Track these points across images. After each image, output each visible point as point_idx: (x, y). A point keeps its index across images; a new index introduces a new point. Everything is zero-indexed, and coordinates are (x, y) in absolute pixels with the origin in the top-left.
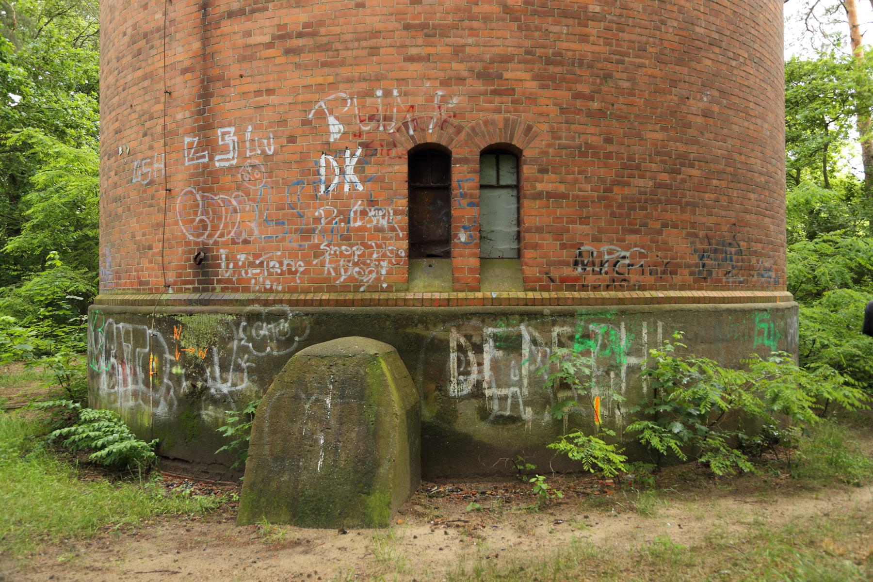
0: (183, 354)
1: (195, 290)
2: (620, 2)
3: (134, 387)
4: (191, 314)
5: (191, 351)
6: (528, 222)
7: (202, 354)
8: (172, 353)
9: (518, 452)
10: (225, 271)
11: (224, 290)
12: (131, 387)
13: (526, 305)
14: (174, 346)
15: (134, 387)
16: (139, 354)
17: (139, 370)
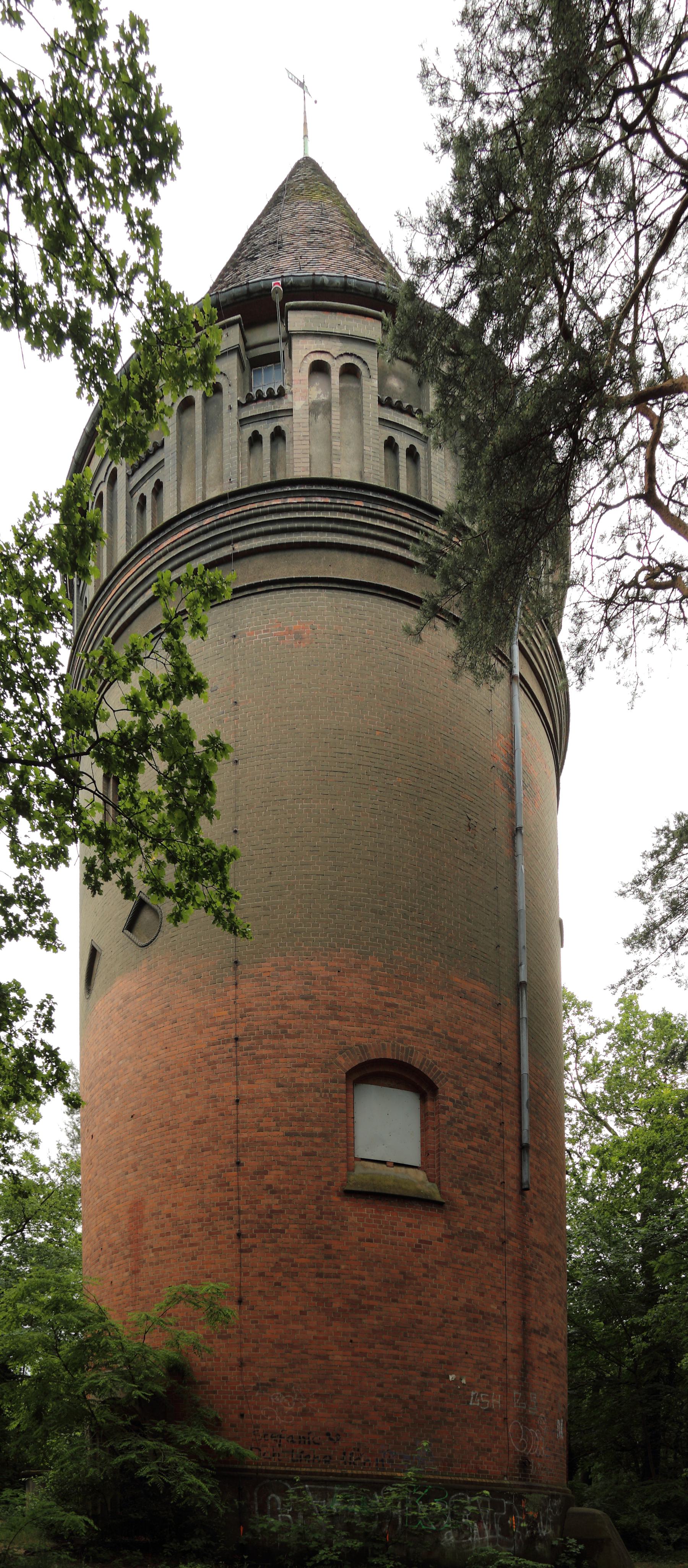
0: (527, 1516)
1: (520, 1480)
2: (686, 1166)
4: (530, 1493)
5: (531, 1514)
6: (586, 593)
7: (536, 1516)
8: (521, 1515)
10: (533, 1471)
12: (488, 1536)
13: (525, 787)
14: (522, 1511)
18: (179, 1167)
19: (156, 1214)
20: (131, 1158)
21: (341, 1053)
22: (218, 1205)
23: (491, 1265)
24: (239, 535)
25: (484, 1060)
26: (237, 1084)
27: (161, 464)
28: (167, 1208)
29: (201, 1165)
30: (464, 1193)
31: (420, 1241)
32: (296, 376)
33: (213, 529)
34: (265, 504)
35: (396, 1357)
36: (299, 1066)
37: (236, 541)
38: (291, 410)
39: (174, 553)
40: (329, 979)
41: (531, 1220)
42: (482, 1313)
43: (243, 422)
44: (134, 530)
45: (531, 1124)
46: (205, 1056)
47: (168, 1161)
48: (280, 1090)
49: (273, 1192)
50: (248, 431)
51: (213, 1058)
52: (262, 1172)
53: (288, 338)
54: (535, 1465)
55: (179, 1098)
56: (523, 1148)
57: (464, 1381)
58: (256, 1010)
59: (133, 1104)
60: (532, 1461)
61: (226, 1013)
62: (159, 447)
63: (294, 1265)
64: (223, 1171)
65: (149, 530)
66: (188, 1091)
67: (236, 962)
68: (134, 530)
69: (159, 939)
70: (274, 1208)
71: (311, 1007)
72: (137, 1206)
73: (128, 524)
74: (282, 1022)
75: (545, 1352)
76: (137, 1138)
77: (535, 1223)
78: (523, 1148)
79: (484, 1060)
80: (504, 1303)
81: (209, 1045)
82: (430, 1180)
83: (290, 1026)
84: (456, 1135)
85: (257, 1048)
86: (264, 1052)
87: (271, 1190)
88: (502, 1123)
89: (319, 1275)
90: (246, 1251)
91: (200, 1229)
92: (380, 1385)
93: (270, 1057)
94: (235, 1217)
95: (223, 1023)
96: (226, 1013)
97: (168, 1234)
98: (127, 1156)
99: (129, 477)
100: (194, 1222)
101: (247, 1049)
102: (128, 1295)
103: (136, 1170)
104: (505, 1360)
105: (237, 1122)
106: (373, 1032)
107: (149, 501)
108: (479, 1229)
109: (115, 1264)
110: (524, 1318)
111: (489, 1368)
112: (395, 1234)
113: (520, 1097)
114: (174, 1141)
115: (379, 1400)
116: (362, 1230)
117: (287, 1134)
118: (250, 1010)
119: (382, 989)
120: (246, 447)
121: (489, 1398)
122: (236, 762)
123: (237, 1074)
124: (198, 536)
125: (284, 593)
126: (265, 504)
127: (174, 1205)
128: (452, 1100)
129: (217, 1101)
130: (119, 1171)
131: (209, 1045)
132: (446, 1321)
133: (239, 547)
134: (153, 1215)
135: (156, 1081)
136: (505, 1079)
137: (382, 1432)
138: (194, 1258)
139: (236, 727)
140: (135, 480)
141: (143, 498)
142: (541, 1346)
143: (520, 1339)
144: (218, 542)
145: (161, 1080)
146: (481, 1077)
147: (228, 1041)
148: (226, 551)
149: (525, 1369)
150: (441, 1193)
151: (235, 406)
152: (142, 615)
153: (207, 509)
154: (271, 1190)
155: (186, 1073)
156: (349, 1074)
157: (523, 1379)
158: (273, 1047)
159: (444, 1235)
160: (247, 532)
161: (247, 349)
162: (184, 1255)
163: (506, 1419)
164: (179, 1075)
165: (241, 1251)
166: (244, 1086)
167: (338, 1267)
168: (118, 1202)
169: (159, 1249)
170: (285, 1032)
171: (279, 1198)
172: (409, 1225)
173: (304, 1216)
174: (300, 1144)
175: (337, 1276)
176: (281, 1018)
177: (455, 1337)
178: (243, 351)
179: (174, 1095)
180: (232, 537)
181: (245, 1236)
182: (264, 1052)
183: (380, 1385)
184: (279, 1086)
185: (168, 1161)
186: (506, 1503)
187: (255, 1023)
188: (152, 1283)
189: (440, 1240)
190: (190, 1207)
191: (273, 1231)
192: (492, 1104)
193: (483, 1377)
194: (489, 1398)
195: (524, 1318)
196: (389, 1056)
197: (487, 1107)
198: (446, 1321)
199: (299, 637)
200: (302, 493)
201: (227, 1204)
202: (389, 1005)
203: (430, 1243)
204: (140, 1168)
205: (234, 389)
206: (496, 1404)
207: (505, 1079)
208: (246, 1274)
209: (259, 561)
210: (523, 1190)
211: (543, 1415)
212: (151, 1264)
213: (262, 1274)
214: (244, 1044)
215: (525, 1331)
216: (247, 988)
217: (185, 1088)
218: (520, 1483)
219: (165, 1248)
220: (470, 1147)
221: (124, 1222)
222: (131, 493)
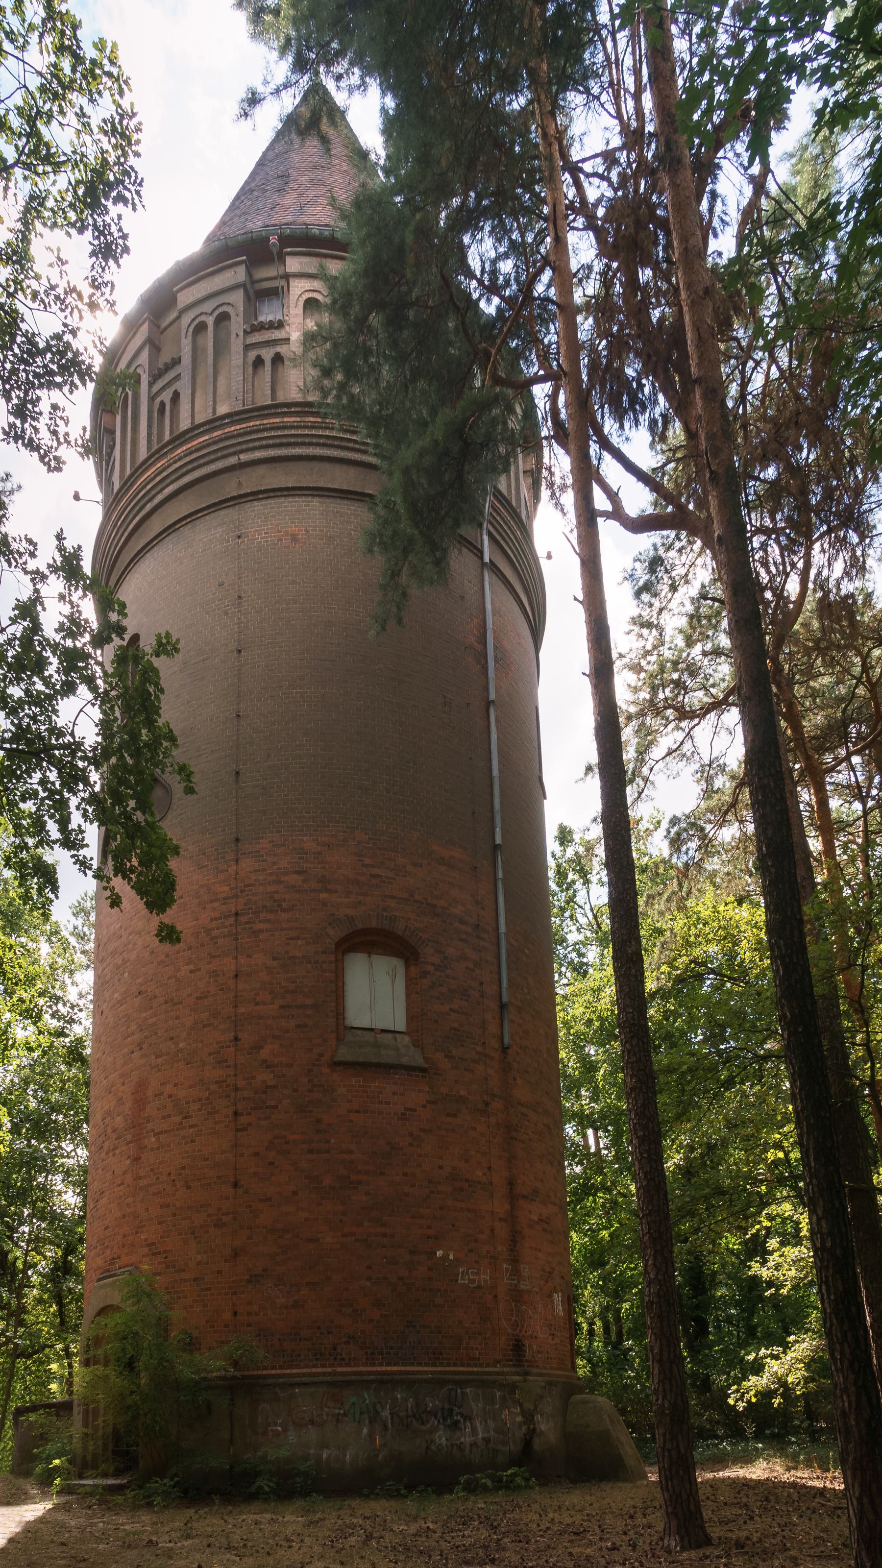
1: (514, 1366)
10: (528, 1355)
18: (181, 1045)
19: (158, 1095)
20: (137, 1037)
21: (330, 924)
22: (217, 1082)
23: (475, 1129)
24: (244, 447)
25: (462, 922)
26: (236, 958)
27: (178, 377)
28: (169, 1088)
29: (202, 1041)
30: (446, 1056)
31: (406, 1109)
32: (293, 311)
33: (221, 440)
34: (265, 422)
35: (384, 1235)
36: (292, 939)
37: (242, 452)
38: (289, 339)
39: (188, 459)
40: (319, 853)
41: (515, 1079)
42: (467, 1181)
43: (247, 348)
44: (155, 439)
45: (509, 981)
46: (208, 931)
47: (172, 1038)
48: (275, 963)
49: (268, 1067)
50: (252, 355)
51: (215, 933)
52: (257, 1047)
53: (287, 277)
54: (530, 1347)
55: (183, 973)
56: (502, 1007)
57: (451, 1257)
58: (253, 885)
59: (140, 980)
60: (527, 1343)
61: (227, 888)
62: (177, 361)
63: (287, 1143)
64: (222, 1047)
65: (167, 437)
66: (191, 967)
67: (237, 840)
68: (155, 439)
69: (169, 816)
70: (270, 1083)
71: (304, 881)
72: (141, 1086)
73: (150, 426)
74: (277, 897)
75: (535, 1218)
76: (144, 1015)
77: (519, 1081)
78: (502, 1007)
79: (462, 922)
80: (489, 1168)
81: (212, 920)
82: (414, 1046)
83: (284, 900)
84: (438, 998)
85: (254, 922)
86: (261, 926)
87: (267, 1065)
88: (481, 984)
89: (311, 1152)
90: (244, 1129)
91: (200, 1110)
92: (369, 1267)
93: (267, 931)
94: (232, 1094)
95: (225, 899)
96: (227, 888)
97: (169, 1116)
98: (133, 1034)
99: (151, 384)
100: (194, 1101)
101: (246, 923)
102: (129, 1186)
103: (141, 1049)
104: (492, 1230)
105: (236, 996)
106: (360, 902)
107: (168, 408)
108: (463, 1093)
109: (117, 1152)
110: (511, 1183)
111: (476, 1241)
112: (381, 1103)
113: (498, 956)
114: (177, 1018)
115: (368, 1284)
116: (349, 1101)
117: (281, 1007)
118: (249, 885)
119: (367, 861)
120: (250, 369)
121: (478, 1274)
122: (240, 651)
123: (237, 948)
124: (209, 445)
125: (282, 499)
126: (265, 422)
127: (176, 1085)
128: (433, 964)
129: (218, 975)
130: (126, 1050)
131: (212, 920)
132: (432, 1192)
133: (244, 457)
134: (156, 1095)
135: (163, 957)
136: (483, 939)
137: (371, 1321)
138: (193, 1141)
139: (239, 619)
140: (156, 388)
141: (162, 404)
142: (530, 1212)
143: (507, 1207)
144: (225, 452)
145: (167, 956)
146: (461, 940)
147: (229, 916)
148: (233, 460)
149: (515, 1238)
150: (425, 1058)
151: (241, 334)
152: (160, 510)
153: (217, 424)
154: (267, 1065)
155: (190, 948)
156: (338, 945)
157: (512, 1250)
158: (269, 921)
159: (428, 1102)
160: (251, 445)
161: (253, 282)
162: (184, 1138)
163: (495, 1296)
164: (184, 950)
165: (237, 1130)
166: (242, 960)
167: (328, 1142)
168: (123, 1084)
169: (160, 1133)
170: (280, 906)
171: (273, 1072)
172: (394, 1093)
173: (296, 1090)
174: (293, 1016)
175: (328, 1152)
176: (277, 892)
177: (441, 1208)
178: (248, 286)
179: (179, 970)
180: (238, 448)
181: (242, 1115)
182: (261, 926)
183: (369, 1267)
184: (274, 959)
185: (172, 1038)
186: (498, 1394)
187: (254, 898)
188: (152, 1170)
189: (424, 1106)
190: (191, 1087)
191: (267, 1107)
192: (471, 966)
193: (471, 1251)
194: (478, 1274)
195: (511, 1183)
196: (374, 924)
197: (467, 968)
198: (432, 1192)
199: (294, 538)
200: (297, 414)
201: (226, 1081)
202: (372, 876)
203: (415, 1110)
204: (145, 1046)
205: (241, 319)
206: (485, 1281)
207: (483, 939)
208: (242, 1155)
209: (261, 470)
210: (505, 1049)
211: (536, 1289)
212: (152, 1150)
213: (256, 1154)
214: (243, 919)
215: (513, 1197)
216: (247, 864)
217: (188, 964)
218: (514, 1369)
219: (166, 1132)
220: (451, 1010)
221: (127, 1105)
222: (152, 399)
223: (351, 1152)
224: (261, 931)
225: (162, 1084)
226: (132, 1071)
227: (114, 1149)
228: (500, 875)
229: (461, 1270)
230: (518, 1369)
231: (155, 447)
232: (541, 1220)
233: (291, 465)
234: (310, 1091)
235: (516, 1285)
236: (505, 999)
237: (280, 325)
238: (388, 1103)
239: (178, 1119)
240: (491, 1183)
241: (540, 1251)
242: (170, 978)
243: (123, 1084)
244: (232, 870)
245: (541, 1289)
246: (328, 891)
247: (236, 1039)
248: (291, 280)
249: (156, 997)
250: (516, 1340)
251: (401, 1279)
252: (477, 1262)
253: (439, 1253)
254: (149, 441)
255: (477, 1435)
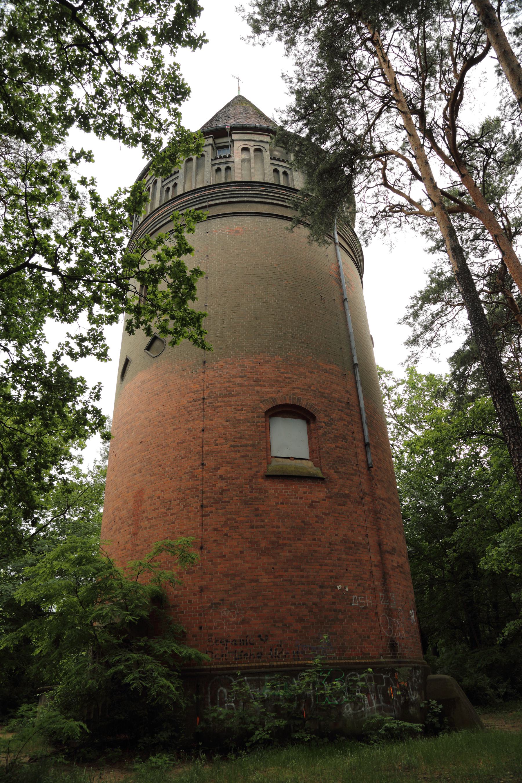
0: (400, 685)
1: (392, 657)
3: (377, 705)
8: (396, 685)
9: (395, 206)
10: (399, 650)
11: (400, 657)
12: (375, 706)
13: (346, 283)
15: (377, 705)
16: (380, 688)
17: (380, 696)
18: (167, 469)
22: (189, 489)
23: (356, 513)
25: (340, 401)
26: (203, 421)
28: (158, 493)
29: (180, 467)
30: (335, 472)
31: (313, 502)
35: (302, 577)
40: (254, 367)
41: (376, 485)
42: (353, 543)
46: (185, 408)
47: (161, 466)
48: (228, 423)
49: (223, 479)
50: (215, 167)
51: (189, 409)
52: (217, 468)
56: (366, 445)
57: (347, 589)
59: (142, 436)
60: (398, 642)
63: (236, 522)
66: (175, 427)
69: (164, 353)
72: (140, 492)
74: (228, 389)
77: (379, 486)
78: (366, 445)
79: (340, 401)
80: (366, 535)
82: (315, 466)
83: (233, 391)
84: (328, 440)
86: (219, 404)
87: (222, 478)
91: (178, 505)
92: (293, 597)
94: (200, 496)
97: (158, 509)
98: (136, 464)
99: (162, 182)
100: (174, 500)
101: (209, 403)
102: (129, 550)
104: (371, 572)
105: (203, 441)
106: (279, 391)
108: (347, 492)
109: (122, 531)
110: (380, 544)
111: (362, 579)
112: (297, 498)
114: (165, 454)
115: (293, 607)
117: (232, 446)
119: (282, 370)
121: (364, 599)
123: (203, 416)
128: (324, 422)
129: (191, 431)
130: (131, 474)
132: (332, 550)
133: (210, 203)
137: (296, 631)
138: (173, 523)
141: (168, 188)
142: (392, 561)
143: (379, 558)
146: (339, 410)
147: (199, 400)
149: (385, 577)
151: (210, 160)
154: (222, 478)
156: (266, 412)
157: (384, 584)
159: (326, 497)
162: (167, 521)
163: (377, 613)
165: (203, 516)
166: (207, 422)
167: (263, 521)
168: (128, 492)
169: (152, 519)
171: (227, 482)
172: (305, 493)
174: (239, 451)
176: (229, 387)
177: (338, 560)
181: (206, 507)
182: (219, 404)
183: (293, 597)
184: (227, 421)
185: (161, 466)
188: (145, 541)
189: (324, 500)
190: (172, 492)
192: (346, 423)
193: (359, 585)
194: (364, 599)
195: (380, 544)
196: (288, 402)
198: (332, 550)
199: (237, 232)
200: (239, 186)
201: (195, 488)
202: (285, 378)
203: (318, 502)
205: (210, 155)
208: (206, 530)
210: (369, 468)
211: (400, 608)
212: (146, 528)
213: (216, 529)
215: (381, 552)
216: (210, 374)
217: (173, 425)
218: (392, 660)
219: (155, 518)
220: (336, 447)
223: (279, 527)
224: (219, 407)
225: (155, 491)
226: (134, 485)
227: (120, 529)
228: (358, 378)
229: (353, 597)
230: (395, 660)
231: (163, 202)
232: (398, 566)
233: (235, 205)
234: (250, 492)
235: (388, 606)
236: (367, 441)
237: (230, 156)
238: (301, 498)
239: (163, 510)
240: (368, 544)
241: (400, 584)
242: (161, 433)
243: (128, 492)
244: (201, 376)
245: (403, 608)
246: (259, 385)
247: (203, 464)
248: (235, 142)
249: (151, 444)
250: (391, 641)
251: (314, 604)
252: (363, 592)
253: (339, 587)
254: (161, 199)
255: (373, 705)
